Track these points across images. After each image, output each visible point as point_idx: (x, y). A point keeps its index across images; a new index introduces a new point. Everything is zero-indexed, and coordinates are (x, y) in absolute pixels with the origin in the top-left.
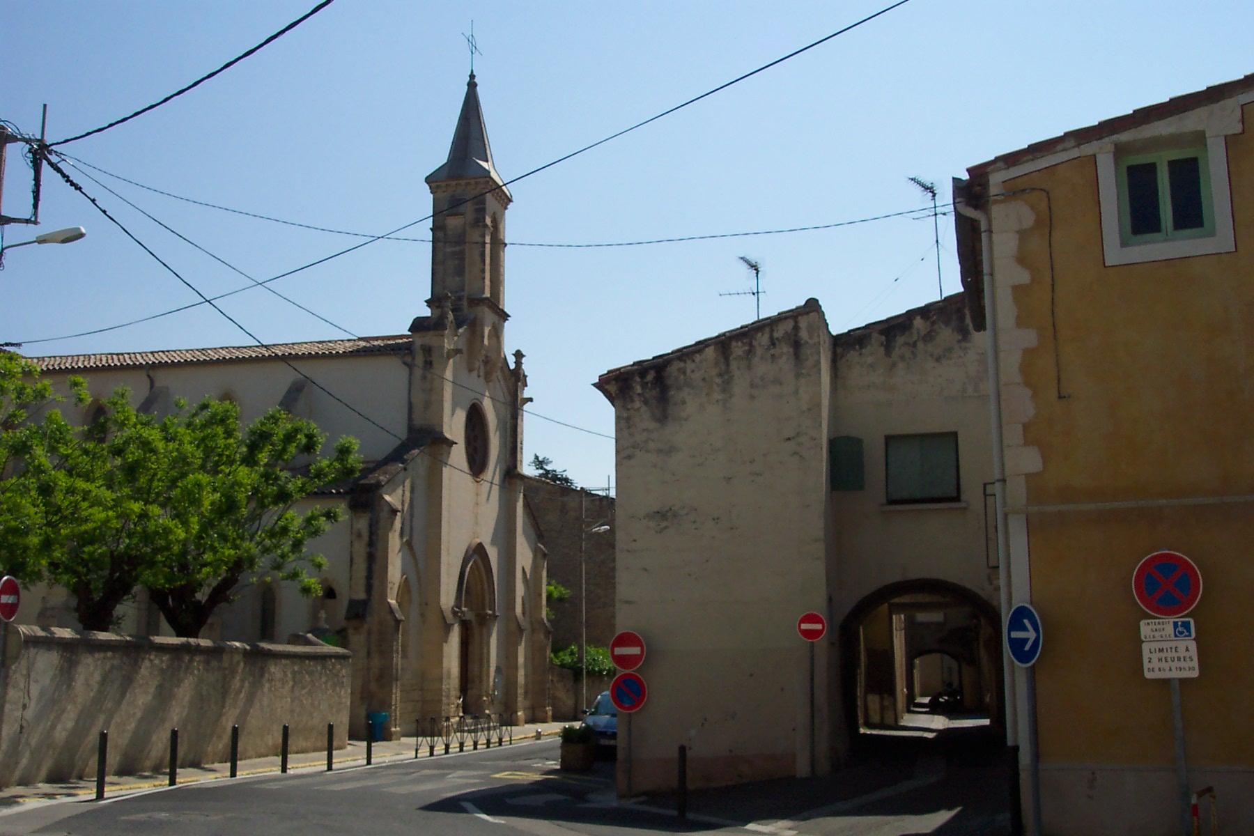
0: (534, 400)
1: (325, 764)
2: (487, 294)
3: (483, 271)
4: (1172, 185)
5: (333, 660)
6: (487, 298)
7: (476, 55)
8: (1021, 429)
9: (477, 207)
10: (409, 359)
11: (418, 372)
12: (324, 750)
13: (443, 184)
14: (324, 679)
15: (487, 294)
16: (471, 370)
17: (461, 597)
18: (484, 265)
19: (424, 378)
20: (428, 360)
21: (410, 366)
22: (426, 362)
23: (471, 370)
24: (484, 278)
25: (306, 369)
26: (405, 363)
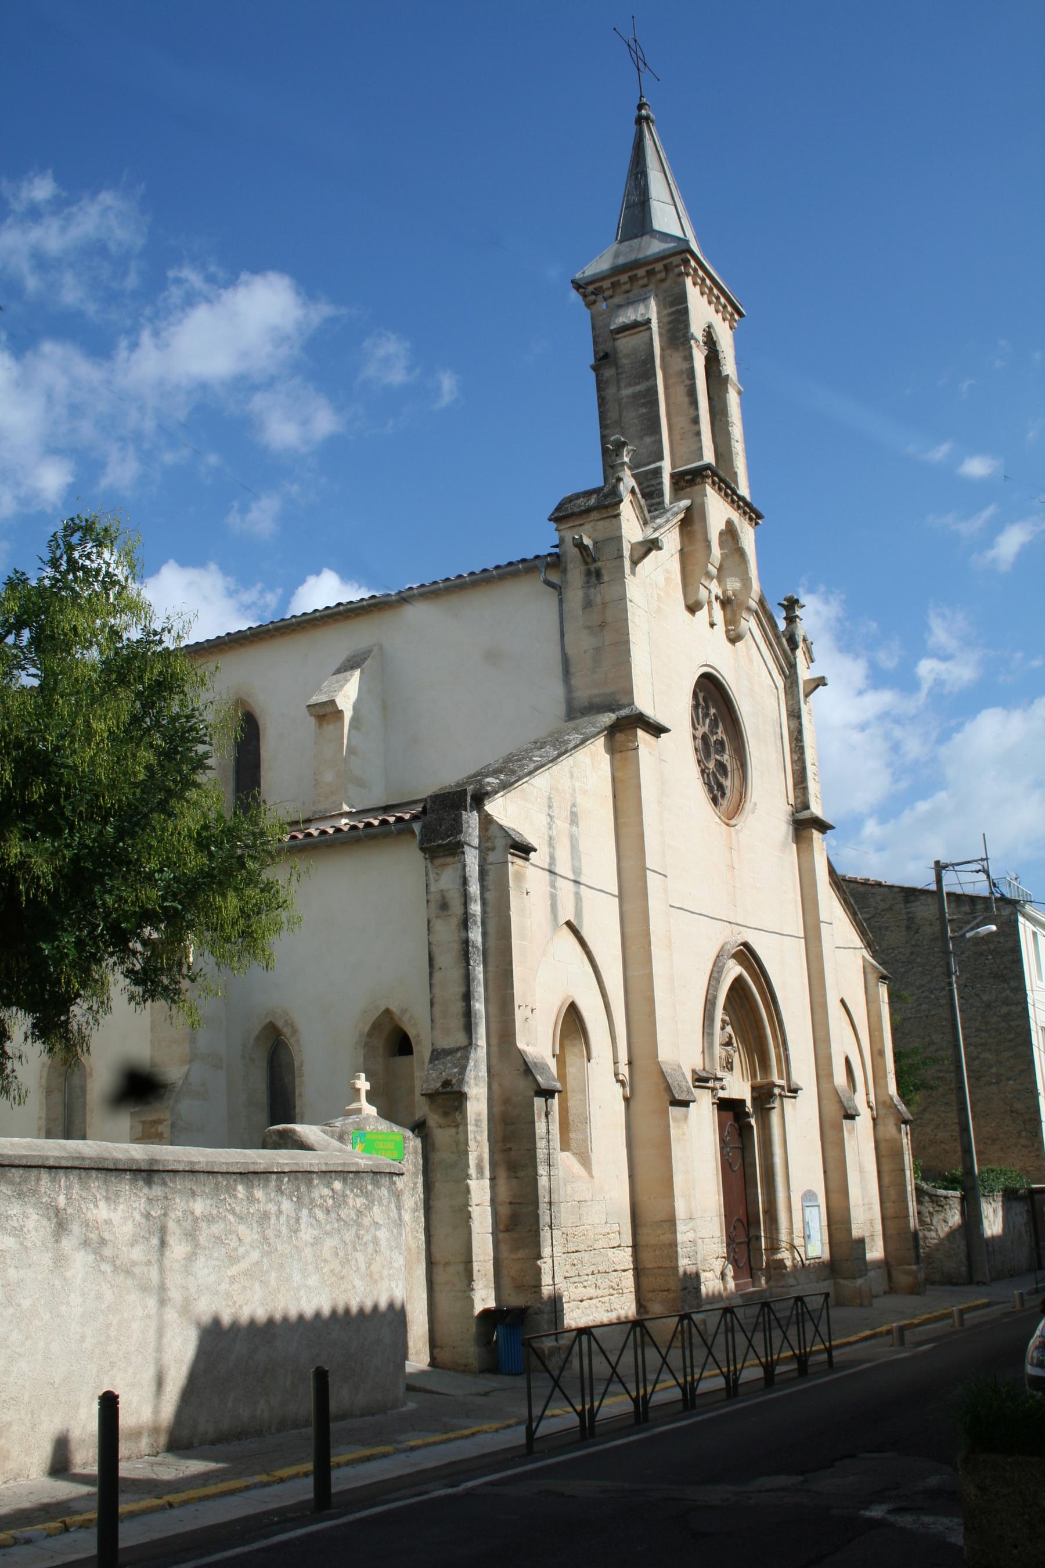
0: (829, 681)
1: (306, 1475)
2: (709, 457)
3: (696, 421)
4: (1024, 979)
5: (338, 1185)
6: (708, 467)
7: (646, 75)
8: (848, 1121)
9: (674, 309)
10: (554, 578)
11: (575, 595)
12: (122, 1549)
13: (606, 284)
14: (307, 1233)
15: (709, 457)
16: (693, 608)
17: (781, 1067)
18: (696, 408)
19: (588, 604)
20: (592, 567)
21: (558, 588)
22: (588, 573)
23: (693, 608)
24: (698, 434)
25: (884, 1151)
26: (548, 583)
